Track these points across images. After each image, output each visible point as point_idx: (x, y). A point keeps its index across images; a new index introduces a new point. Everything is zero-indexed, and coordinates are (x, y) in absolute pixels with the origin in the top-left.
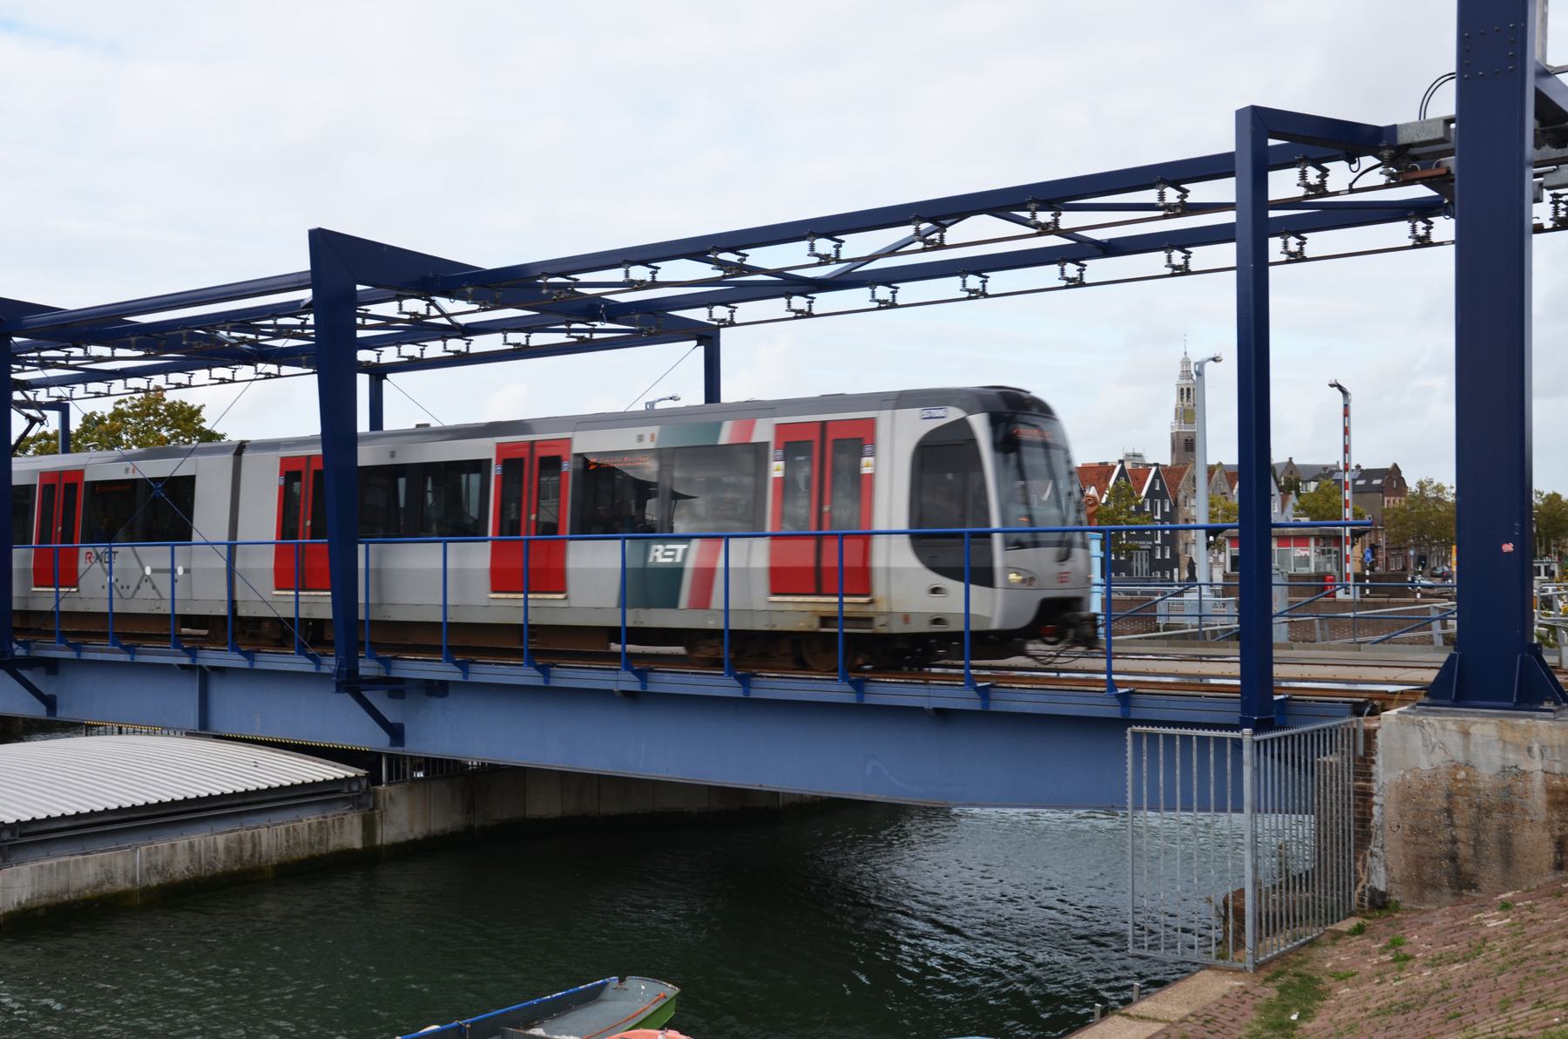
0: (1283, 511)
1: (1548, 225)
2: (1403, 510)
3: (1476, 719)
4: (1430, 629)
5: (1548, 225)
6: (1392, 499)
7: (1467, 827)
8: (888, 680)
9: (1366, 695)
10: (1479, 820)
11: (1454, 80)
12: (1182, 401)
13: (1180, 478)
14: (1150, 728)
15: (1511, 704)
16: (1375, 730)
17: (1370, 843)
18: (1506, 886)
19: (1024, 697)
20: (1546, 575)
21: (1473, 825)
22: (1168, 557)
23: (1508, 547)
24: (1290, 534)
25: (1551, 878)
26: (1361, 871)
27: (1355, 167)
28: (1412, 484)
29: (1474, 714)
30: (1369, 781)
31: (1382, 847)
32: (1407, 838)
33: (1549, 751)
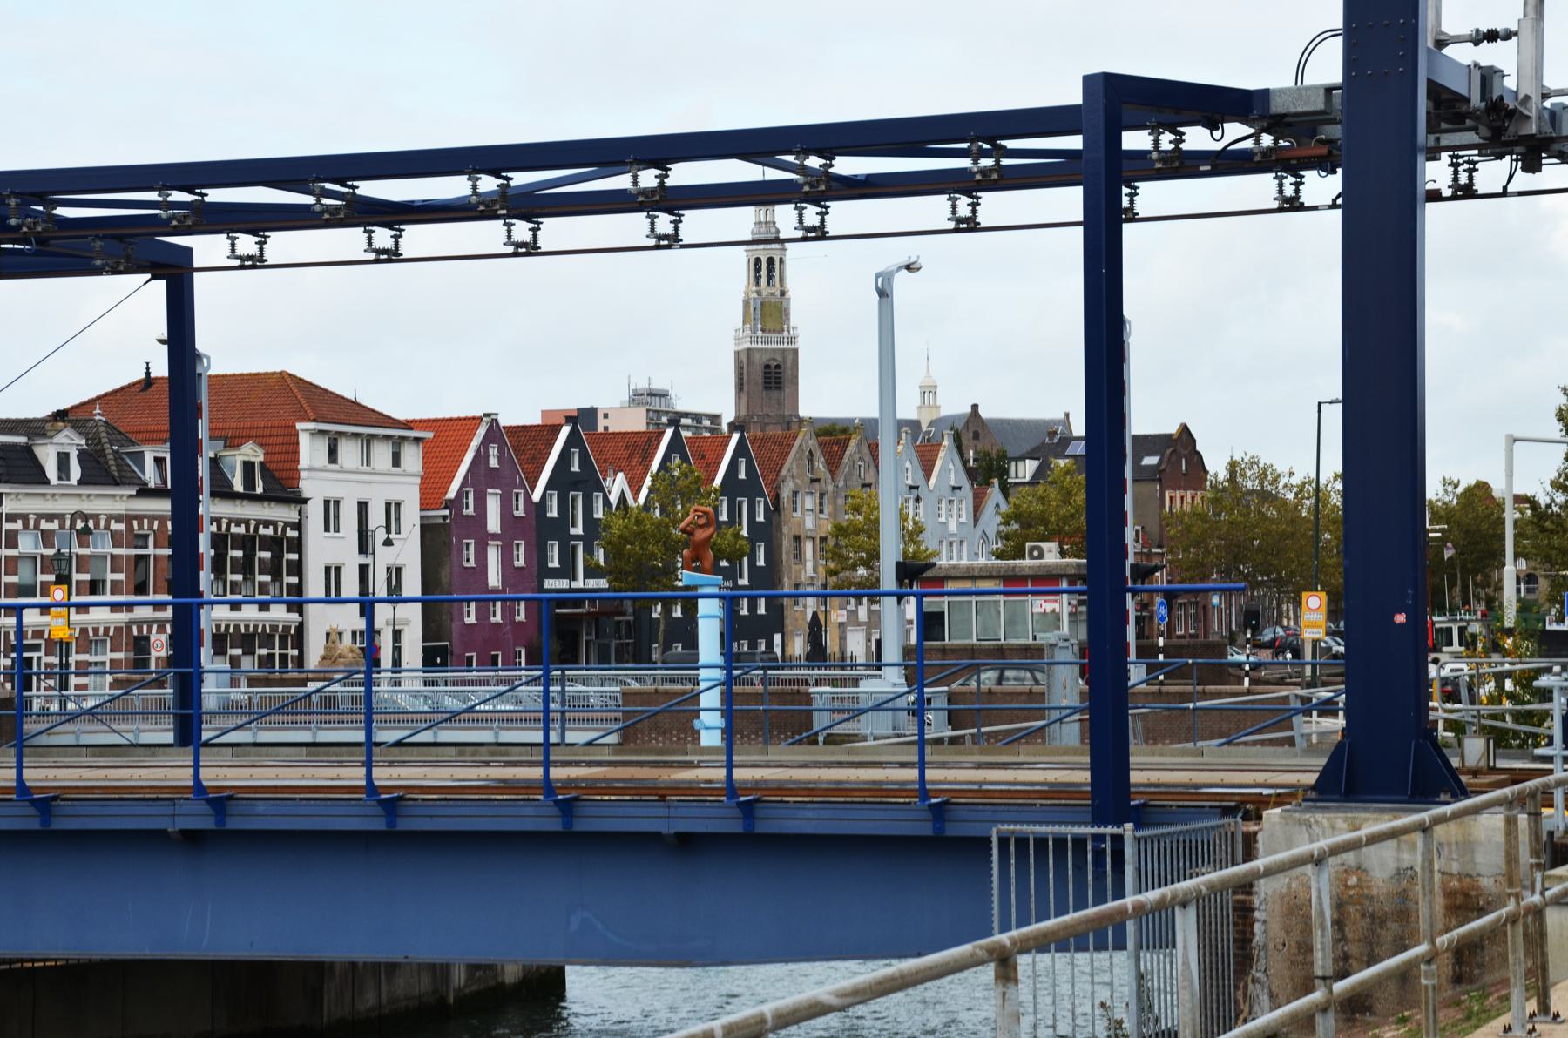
0: (976, 520)
1: (1447, 192)
2: (1202, 517)
3: (1367, 815)
4: (1291, 729)
5: (1447, 192)
6: (1178, 494)
7: (1360, 940)
8: (606, 798)
9: (1237, 798)
10: (1373, 932)
11: (1341, 37)
12: (758, 284)
13: (784, 455)
14: (1018, 827)
15: (1406, 798)
16: (1255, 833)
17: (1252, 968)
18: (1402, 1005)
19: (800, 814)
20: (1461, 645)
21: (1366, 938)
22: (762, 611)
23: (1400, 618)
24: (1027, 572)
25: (1450, 992)
26: (1241, 1001)
27: (1217, 134)
28: (1216, 466)
29: (1366, 810)
30: (1250, 893)
31: (1265, 970)
32: (1293, 958)
33: (1446, 849)
